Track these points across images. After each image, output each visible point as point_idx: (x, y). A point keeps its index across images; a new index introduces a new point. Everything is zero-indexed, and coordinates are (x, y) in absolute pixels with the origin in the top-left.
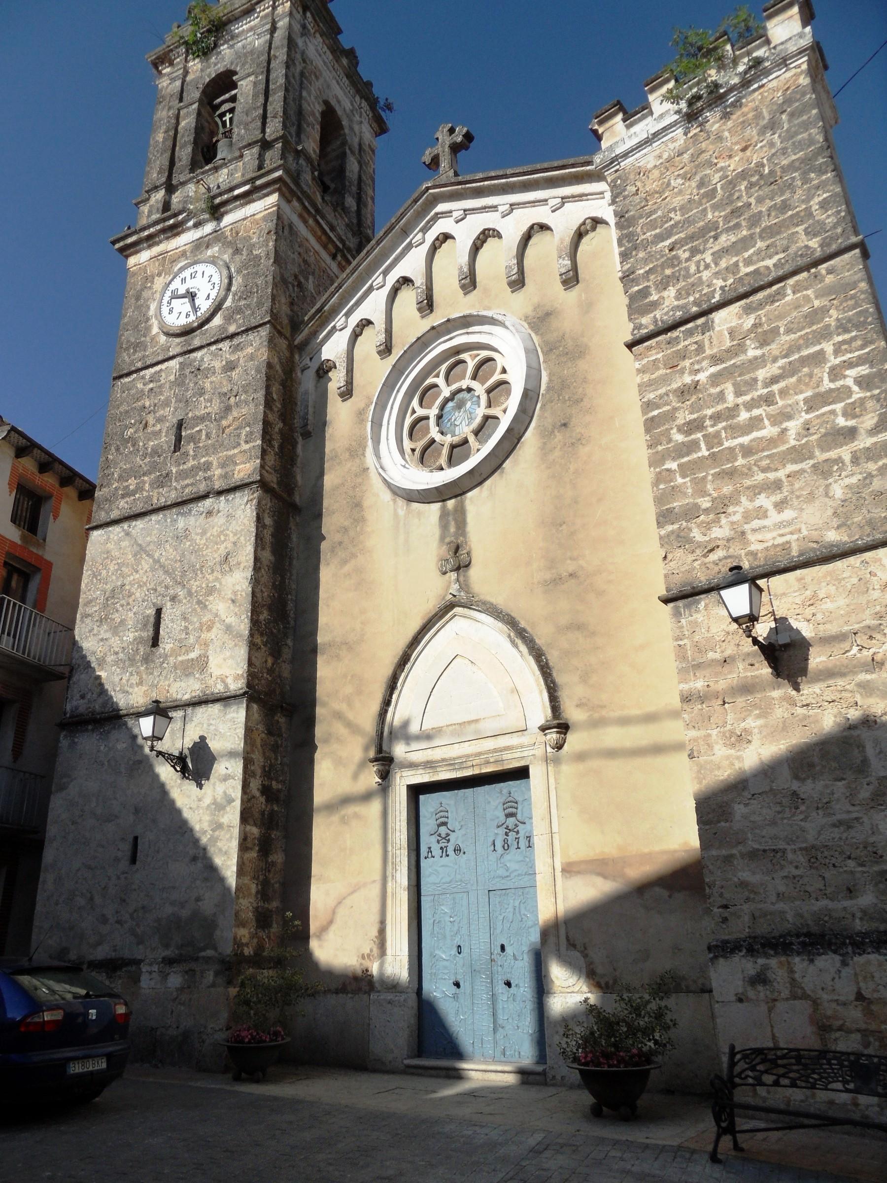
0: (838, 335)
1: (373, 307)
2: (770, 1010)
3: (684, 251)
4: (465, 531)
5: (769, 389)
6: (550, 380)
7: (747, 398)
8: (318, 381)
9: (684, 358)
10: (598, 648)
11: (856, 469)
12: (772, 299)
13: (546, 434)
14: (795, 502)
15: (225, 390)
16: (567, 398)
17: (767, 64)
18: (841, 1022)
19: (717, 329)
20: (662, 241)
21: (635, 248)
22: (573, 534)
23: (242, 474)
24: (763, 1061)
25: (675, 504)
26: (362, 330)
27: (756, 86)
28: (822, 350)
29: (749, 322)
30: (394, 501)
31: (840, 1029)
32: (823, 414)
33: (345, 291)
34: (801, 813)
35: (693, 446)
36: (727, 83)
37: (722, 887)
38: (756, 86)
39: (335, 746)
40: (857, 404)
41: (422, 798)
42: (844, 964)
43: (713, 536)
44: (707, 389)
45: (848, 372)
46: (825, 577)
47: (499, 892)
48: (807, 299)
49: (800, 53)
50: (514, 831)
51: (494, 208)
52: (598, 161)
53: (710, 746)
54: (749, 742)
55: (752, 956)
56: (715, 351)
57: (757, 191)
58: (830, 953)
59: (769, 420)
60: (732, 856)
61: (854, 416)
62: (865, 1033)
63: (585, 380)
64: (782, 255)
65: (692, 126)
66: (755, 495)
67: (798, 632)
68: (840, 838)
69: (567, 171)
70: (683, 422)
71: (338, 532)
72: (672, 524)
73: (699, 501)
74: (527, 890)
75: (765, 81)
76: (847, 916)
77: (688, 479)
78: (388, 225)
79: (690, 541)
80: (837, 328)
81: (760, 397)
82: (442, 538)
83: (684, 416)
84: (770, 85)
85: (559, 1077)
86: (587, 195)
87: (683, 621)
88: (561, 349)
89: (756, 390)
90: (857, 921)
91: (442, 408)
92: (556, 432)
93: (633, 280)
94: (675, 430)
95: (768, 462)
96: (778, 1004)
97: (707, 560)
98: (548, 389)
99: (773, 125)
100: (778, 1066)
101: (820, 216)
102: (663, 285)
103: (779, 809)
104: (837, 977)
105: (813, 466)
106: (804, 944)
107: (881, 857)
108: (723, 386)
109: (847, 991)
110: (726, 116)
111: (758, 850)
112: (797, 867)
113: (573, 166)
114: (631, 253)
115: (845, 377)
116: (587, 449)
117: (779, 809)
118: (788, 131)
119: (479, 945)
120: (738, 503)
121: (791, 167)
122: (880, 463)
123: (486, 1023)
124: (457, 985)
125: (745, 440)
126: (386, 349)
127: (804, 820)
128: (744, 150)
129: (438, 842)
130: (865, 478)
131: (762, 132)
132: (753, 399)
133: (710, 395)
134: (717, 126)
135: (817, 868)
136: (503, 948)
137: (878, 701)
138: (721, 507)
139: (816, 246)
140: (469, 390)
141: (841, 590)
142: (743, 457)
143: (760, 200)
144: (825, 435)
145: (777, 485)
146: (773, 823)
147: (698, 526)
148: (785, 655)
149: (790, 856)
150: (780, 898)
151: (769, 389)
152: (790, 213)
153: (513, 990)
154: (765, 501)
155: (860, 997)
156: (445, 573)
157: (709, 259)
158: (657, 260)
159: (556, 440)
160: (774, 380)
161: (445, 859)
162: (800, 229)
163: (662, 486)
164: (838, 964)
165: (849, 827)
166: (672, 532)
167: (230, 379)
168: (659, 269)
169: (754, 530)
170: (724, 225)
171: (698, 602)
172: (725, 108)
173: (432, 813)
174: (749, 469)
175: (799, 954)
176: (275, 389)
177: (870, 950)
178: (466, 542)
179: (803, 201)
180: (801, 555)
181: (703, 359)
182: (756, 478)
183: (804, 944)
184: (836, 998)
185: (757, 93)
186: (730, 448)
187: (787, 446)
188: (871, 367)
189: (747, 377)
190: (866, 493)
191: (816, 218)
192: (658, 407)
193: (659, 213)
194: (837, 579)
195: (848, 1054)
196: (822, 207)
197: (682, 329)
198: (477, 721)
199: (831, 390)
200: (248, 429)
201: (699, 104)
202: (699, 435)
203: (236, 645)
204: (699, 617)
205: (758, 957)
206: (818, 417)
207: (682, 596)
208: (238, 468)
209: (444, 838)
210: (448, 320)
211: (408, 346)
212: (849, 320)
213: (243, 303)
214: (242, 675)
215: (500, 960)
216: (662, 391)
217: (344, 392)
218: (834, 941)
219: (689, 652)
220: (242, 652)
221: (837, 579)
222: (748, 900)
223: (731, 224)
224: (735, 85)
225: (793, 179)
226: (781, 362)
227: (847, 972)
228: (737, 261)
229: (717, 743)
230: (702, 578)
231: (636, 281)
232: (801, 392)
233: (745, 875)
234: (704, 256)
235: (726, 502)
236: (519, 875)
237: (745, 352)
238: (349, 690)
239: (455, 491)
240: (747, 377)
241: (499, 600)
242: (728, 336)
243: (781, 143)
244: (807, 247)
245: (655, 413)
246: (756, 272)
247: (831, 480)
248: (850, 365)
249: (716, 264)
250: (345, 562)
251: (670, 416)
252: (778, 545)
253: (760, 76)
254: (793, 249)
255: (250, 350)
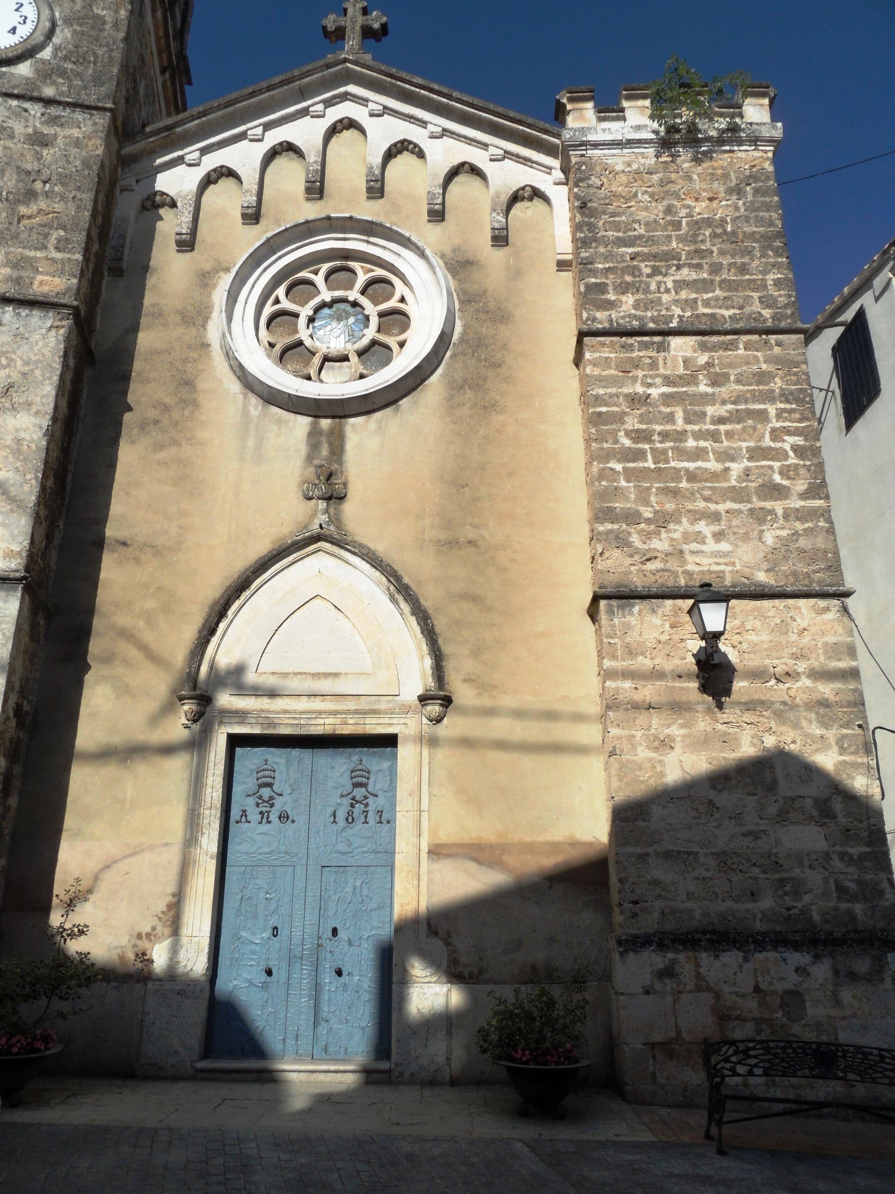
0: (781, 402)
1: (244, 156)
2: (675, 1002)
3: (646, 266)
4: (341, 458)
5: (716, 427)
6: (464, 333)
7: (696, 428)
8: (141, 212)
9: (637, 367)
10: (494, 625)
11: (787, 525)
12: (726, 347)
13: (456, 387)
14: (732, 538)
15: (29, 167)
16: (483, 357)
17: (742, 135)
18: (739, 1012)
19: (672, 352)
20: (625, 246)
21: (595, 240)
22: (476, 500)
23: (45, 289)
24: (736, 1052)
25: (617, 505)
26: (218, 178)
27: (727, 148)
28: (766, 410)
29: (703, 359)
30: (245, 397)
31: (738, 1018)
32: (763, 467)
33: (208, 122)
34: (715, 820)
35: (640, 455)
36: (706, 131)
37: (634, 883)
38: (727, 148)
39: (119, 670)
40: (792, 468)
41: (239, 751)
42: (746, 959)
43: (652, 546)
44: (657, 406)
45: (786, 438)
46: (753, 611)
47: (334, 869)
48: (756, 359)
49: (770, 141)
50: (367, 806)
51: (423, 124)
52: (568, 136)
53: (634, 747)
54: (672, 748)
55: (662, 950)
56: (669, 372)
57: (720, 243)
58: (734, 949)
59: (714, 454)
60: (647, 855)
61: (789, 478)
62: (758, 1021)
63: (504, 347)
64: (738, 312)
65: (664, 153)
66: (696, 520)
67: (725, 655)
68: (748, 847)
69: (521, 128)
70: (631, 428)
71: (154, 407)
72: (612, 523)
73: (642, 509)
74: (373, 869)
75: (736, 148)
76: (749, 917)
77: (632, 485)
78: (288, 75)
79: (629, 544)
80: (781, 396)
81: (707, 430)
82: (309, 459)
83: (632, 423)
84: (740, 155)
85: (407, 1075)
86: (533, 162)
87: (616, 621)
88: (481, 305)
89: (705, 424)
90: (758, 921)
91: (317, 310)
92: (467, 388)
93: (590, 270)
94: (622, 433)
95: (710, 493)
96: (683, 996)
97: (645, 567)
98: (462, 340)
99: (738, 191)
100: (750, 1057)
101: (772, 291)
102: (623, 289)
103: (695, 814)
104: (739, 971)
105: (750, 509)
106: (711, 941)
107: (781, 866)
108: (673, 409)
109: (746, 983)
110: (697, 160)
111: (673, 851)
112: (707, 870)
113: (529, 126)
114: (591, 243)
115: (784, 441)
116: (501, 418)
117: (695, 814)
118: (752, 202)
119: (302, 928)
120: (679, 522)
121: (751, 236)
122: (806, 525)
123: (305, 1019)
124: (269, 972)
125: (691, 466)
126: (253, 216)
127: (718, 827)
128: (711, 199)
129: (258, 805)
130: (793, 535)
131: (730, 191)
132: (700, 430)
133: (660, 412)
134: (686, 165)
135: (725, 872)
136: (335, 931)
137: (789, 730)
138: (662, 521)
139: (768, 316)
140: (355, 304)
141: (765, 626)
142: (687, 481)
143: (722, 253)
144: (763, 485)
145: (716, 517)
146: (690, 827)
147: (638, 533)
148: (714, 674)
149: (702, 859)
150: (690, 896)
151: (716, 427)
152: (748, 277)
153: (344, 978)
154: (704, 528)
155: (757, 989)
156: (310, 499)
157: (670, 285)
158: (618, 262)
159: (466, 396)
160: (721, 420)
161: (264, 827)
162: (756, 295)
163: (604, 483)
164: (740, 960)
165: (757, 838)
166: (611, 531)
167: (39, 157)
168: (619, 272)
169: (692, 552)
170: (687, 259)
171: (633, 606)
172: (698, 152)
173: (252, 771)
174: (692, 494)
175: (706, 950)
176: (101, 197)
177: (769, 948)
178: (342, 472)
179: (760, 272)
180: (734, 586)
181: (657, 376)
182: (697, 504)
183: (711, 941)
184: (736, 990)
185: (726, 155)
186: (674, 468)
187: (726, 485)
188: (806, 440)
189: (697, 408)
190: (793, 547)
191: (770, 292)
192: (606, 405)
193: (624, 218)
194: (763, 616)
195: (810, 1043)
196: (775, 285)
197: (639, 339)
198: (336, 675)
199: (771, 448)
200: (62, 233)
201: (677, 136)
202: (647, 447)
203: (12, 511)
204: (633, 620)
205: (668, 952)
206: (758, 467)
207: (611, 597)
208: (40, 278)
209: (267, 802)
210: (351, 218)
211: (292, 224)
212: (791, 393)
213: (69, 66)
214: (19, 553)
215: (328, 945)
216: (613, 390)
217: (185, 241)
218: (738, 938)
219: (619, 652)
220: (23, 522)
221: (763, 616)
222: (659, 897)
223: (694, 262)
224: (712, 137)
225: (754, 247)
226: (730, 407)
227: (748, 967)
228: (697, 298)
229: (641, 744)
230: (638, 583)
231: (594, 273)
232: (745, 441)
233: (658, 874)
234: (665, 279)
235: (668, 517)
236: (364, 852)
237: (697, 384)
238: (150, 604)
239: (340, 410)
240: (697, 408)
241: (380, 547)
242: (682, 364)
243: (745, 210)
244: (759, 313)
245: (604, 409)
246: (713, 316)
247: (764, 527)
248: (789, 432)
249: (677, 293)
250: (160, 447)
251: (620, 418)
252: (714, 572)
253: (733, 141)
254: (747, 310)
255: (76, 133)
